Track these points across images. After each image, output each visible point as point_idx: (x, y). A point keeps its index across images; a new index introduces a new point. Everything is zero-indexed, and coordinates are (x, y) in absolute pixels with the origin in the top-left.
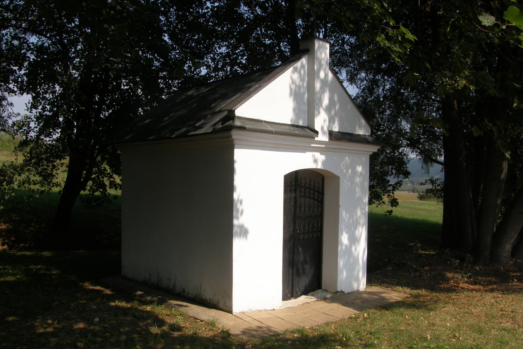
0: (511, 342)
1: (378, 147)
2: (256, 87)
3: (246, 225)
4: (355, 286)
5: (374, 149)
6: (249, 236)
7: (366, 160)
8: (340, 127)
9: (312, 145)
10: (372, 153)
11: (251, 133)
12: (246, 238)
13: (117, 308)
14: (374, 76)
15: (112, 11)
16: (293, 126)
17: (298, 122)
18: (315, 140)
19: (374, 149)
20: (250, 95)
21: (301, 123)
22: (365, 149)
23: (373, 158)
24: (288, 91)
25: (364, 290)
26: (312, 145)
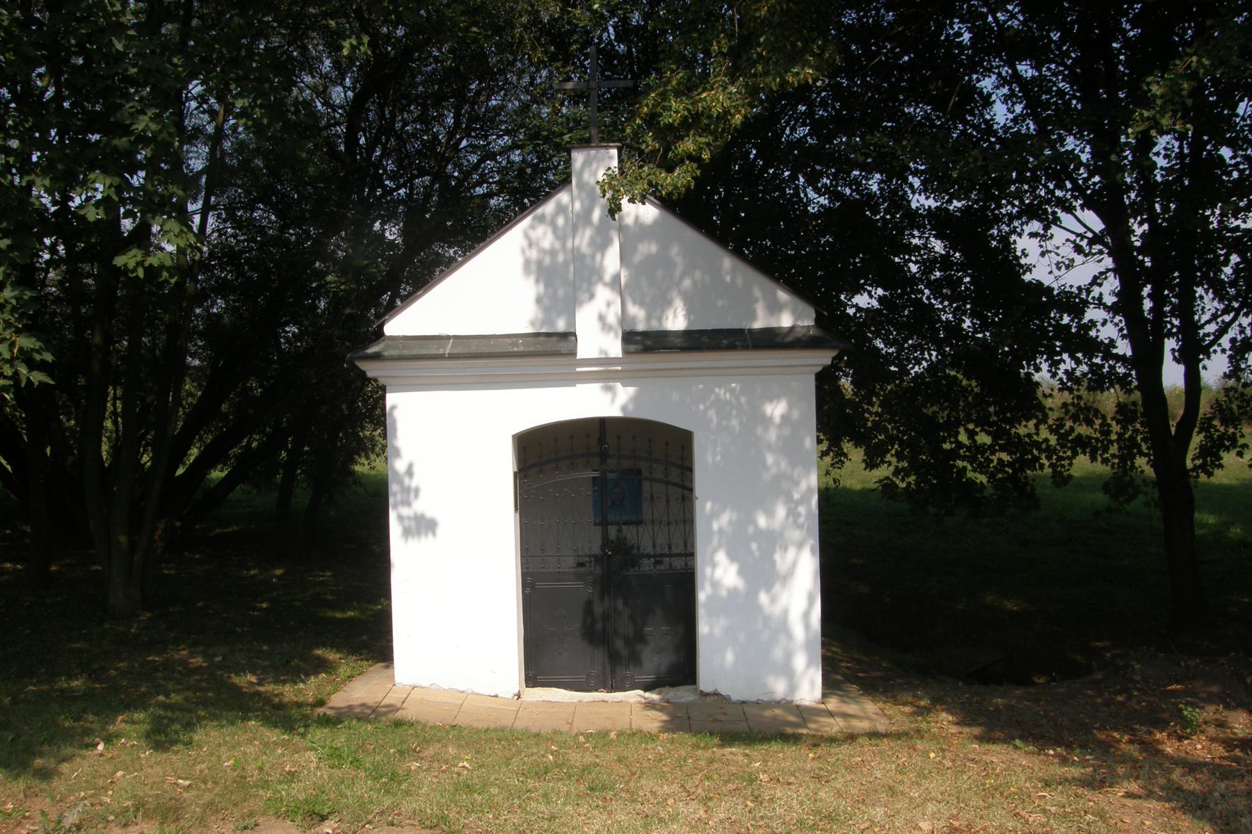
0: (70, 780)
1: (834, 353)
2: (1232, 233)
3: (429, 514)
4: (779, 688)
5: (824, 358)
6: (439, 531)
7: (807, 388)
8: (689, 312)
9: (578, 369)
10: (820, 369)
11: (399, 363)
12: (434, 534)
13: (1172, 691)
14: (935, 120)
15: (83, 245)
16: (537, 335)
17: (551, 322)
18: (578, 358)
19: (824, 358)
20: (776, 280)
21: (676, 321)
22: (780, 362)
23: (825, 380)
24: (519, 262)
25: (814, 705)
26: (578, 369)
